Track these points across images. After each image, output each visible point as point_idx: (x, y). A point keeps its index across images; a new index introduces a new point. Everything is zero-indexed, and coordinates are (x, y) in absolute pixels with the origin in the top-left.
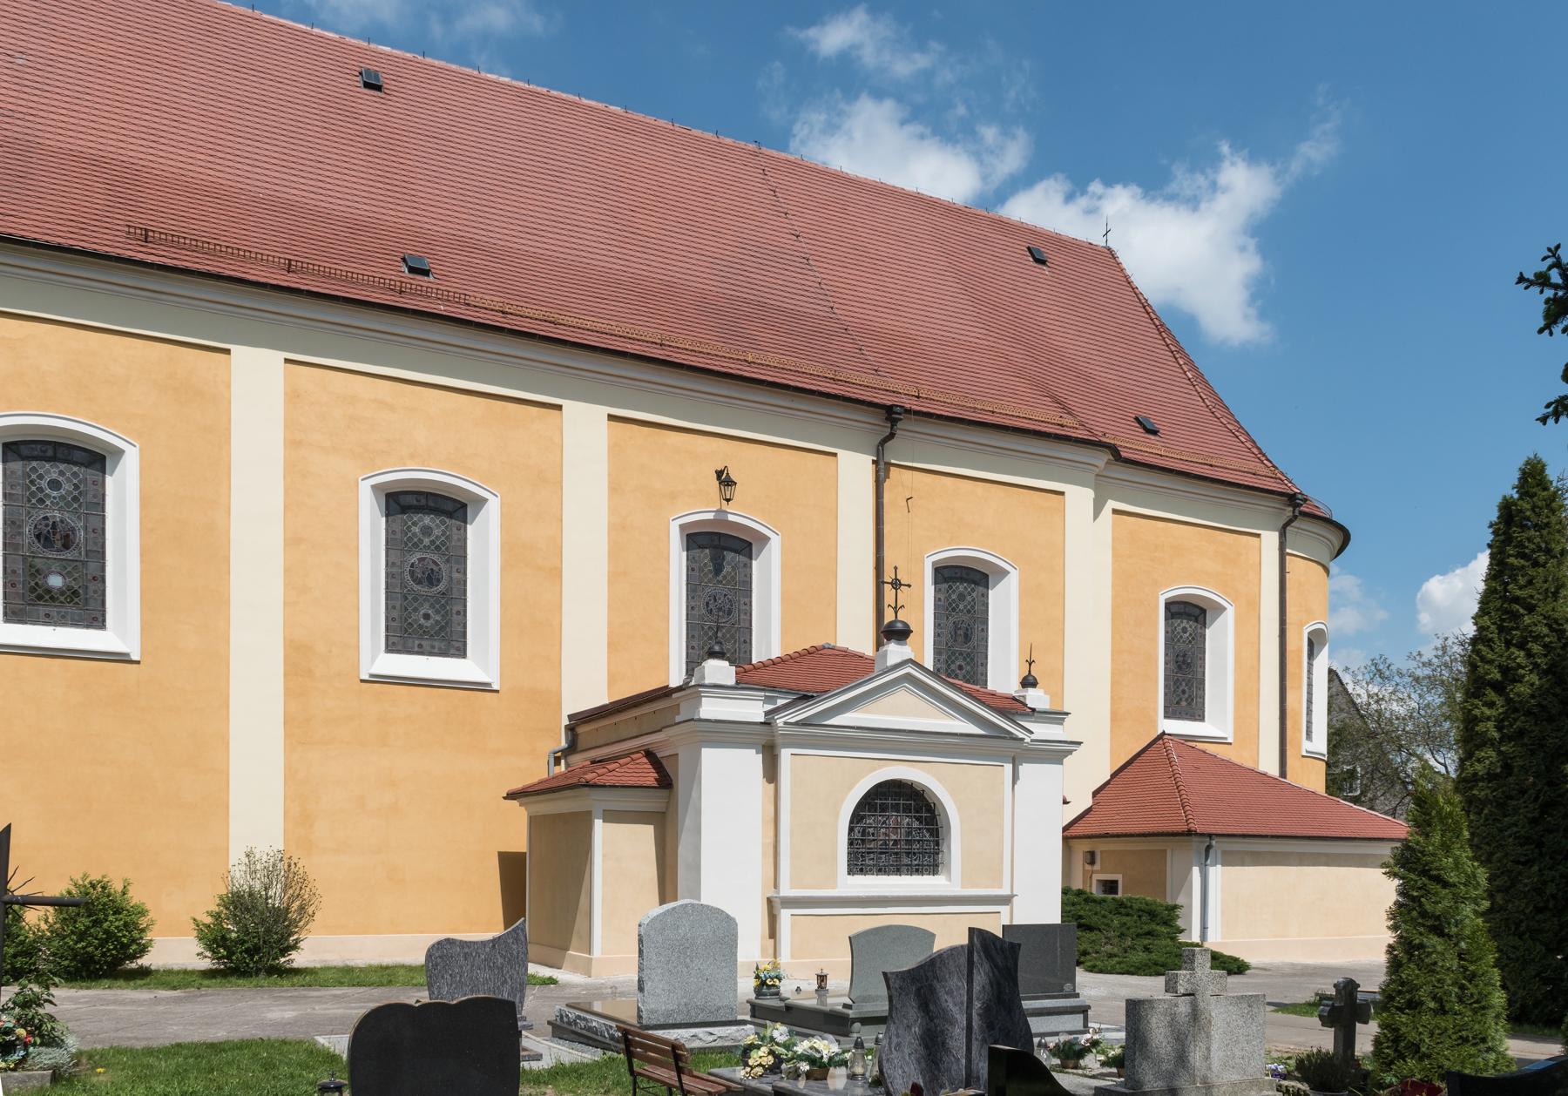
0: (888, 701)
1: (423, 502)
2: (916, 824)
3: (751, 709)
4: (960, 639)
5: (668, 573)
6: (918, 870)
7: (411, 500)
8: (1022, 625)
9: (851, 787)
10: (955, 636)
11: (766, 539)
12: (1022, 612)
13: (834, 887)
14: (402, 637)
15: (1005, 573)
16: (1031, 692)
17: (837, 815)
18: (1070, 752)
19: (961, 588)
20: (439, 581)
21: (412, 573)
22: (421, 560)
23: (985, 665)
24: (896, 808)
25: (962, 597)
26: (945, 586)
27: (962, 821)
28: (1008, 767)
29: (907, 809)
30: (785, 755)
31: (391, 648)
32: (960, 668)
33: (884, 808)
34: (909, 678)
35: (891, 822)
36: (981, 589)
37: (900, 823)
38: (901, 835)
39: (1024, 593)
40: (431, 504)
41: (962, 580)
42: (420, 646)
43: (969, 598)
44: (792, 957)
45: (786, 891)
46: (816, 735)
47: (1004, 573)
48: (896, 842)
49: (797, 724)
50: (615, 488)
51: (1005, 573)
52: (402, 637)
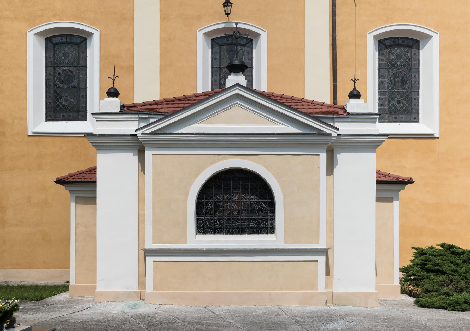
0: (224, 115)
1: (64, 40)
2: (254, 199)
3: (128, 126)
4: (398, 84)
5: (196, 62)
6: (258, 232)
7: (58, 40)
8: (442, 70)
9: (197, 176)
10: (394, 83)
11: (258, 35)
12: (442, 61)
13: (185, 243)
14: (53, 114)
15: (429, 37)
16: (353, 101)
17: (187, 194)
18: (379, 145)
19: (399, 51)
20: (72, 81)
21: (59, 79)
22: (63, 71)
23: (417, 99)
24: (236, 188)
25: (398, 57)
26: (385, 52)
27: (284, 196)
28: (323, 157)
29: (245, 189)
30: (149, 154)
31: (49, 118)
32: (399, 102)
33: (228, 188)
34: (238, 96)
35: (235, 198)
36: (413, 50)
37: (238, 200)
38: (244, 206)
39: (443, 49)
40: (68, 40)
41: (399, 45)
42: (63, 116)
43: (405, 57)
44: (155, 288)
45: (150, 245)
46: (167, 140)
47: (428, 37)
48: (239, 212)
49: (151, 133)
50: (164, 17)
51: (429, 37)
52: (53, 114)
